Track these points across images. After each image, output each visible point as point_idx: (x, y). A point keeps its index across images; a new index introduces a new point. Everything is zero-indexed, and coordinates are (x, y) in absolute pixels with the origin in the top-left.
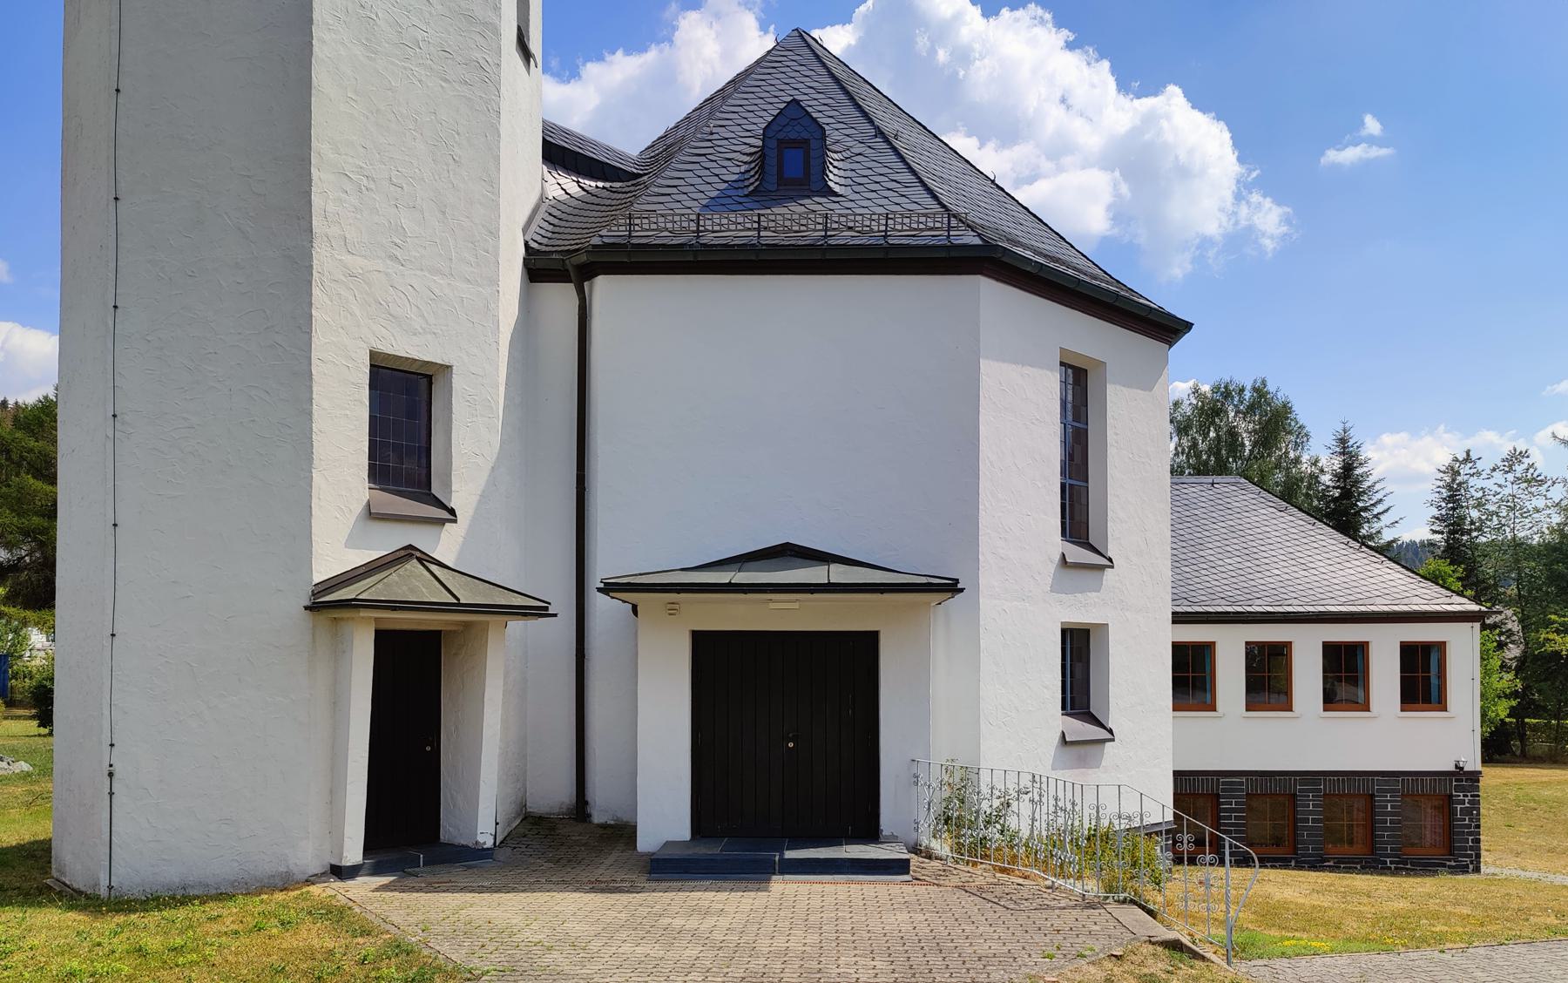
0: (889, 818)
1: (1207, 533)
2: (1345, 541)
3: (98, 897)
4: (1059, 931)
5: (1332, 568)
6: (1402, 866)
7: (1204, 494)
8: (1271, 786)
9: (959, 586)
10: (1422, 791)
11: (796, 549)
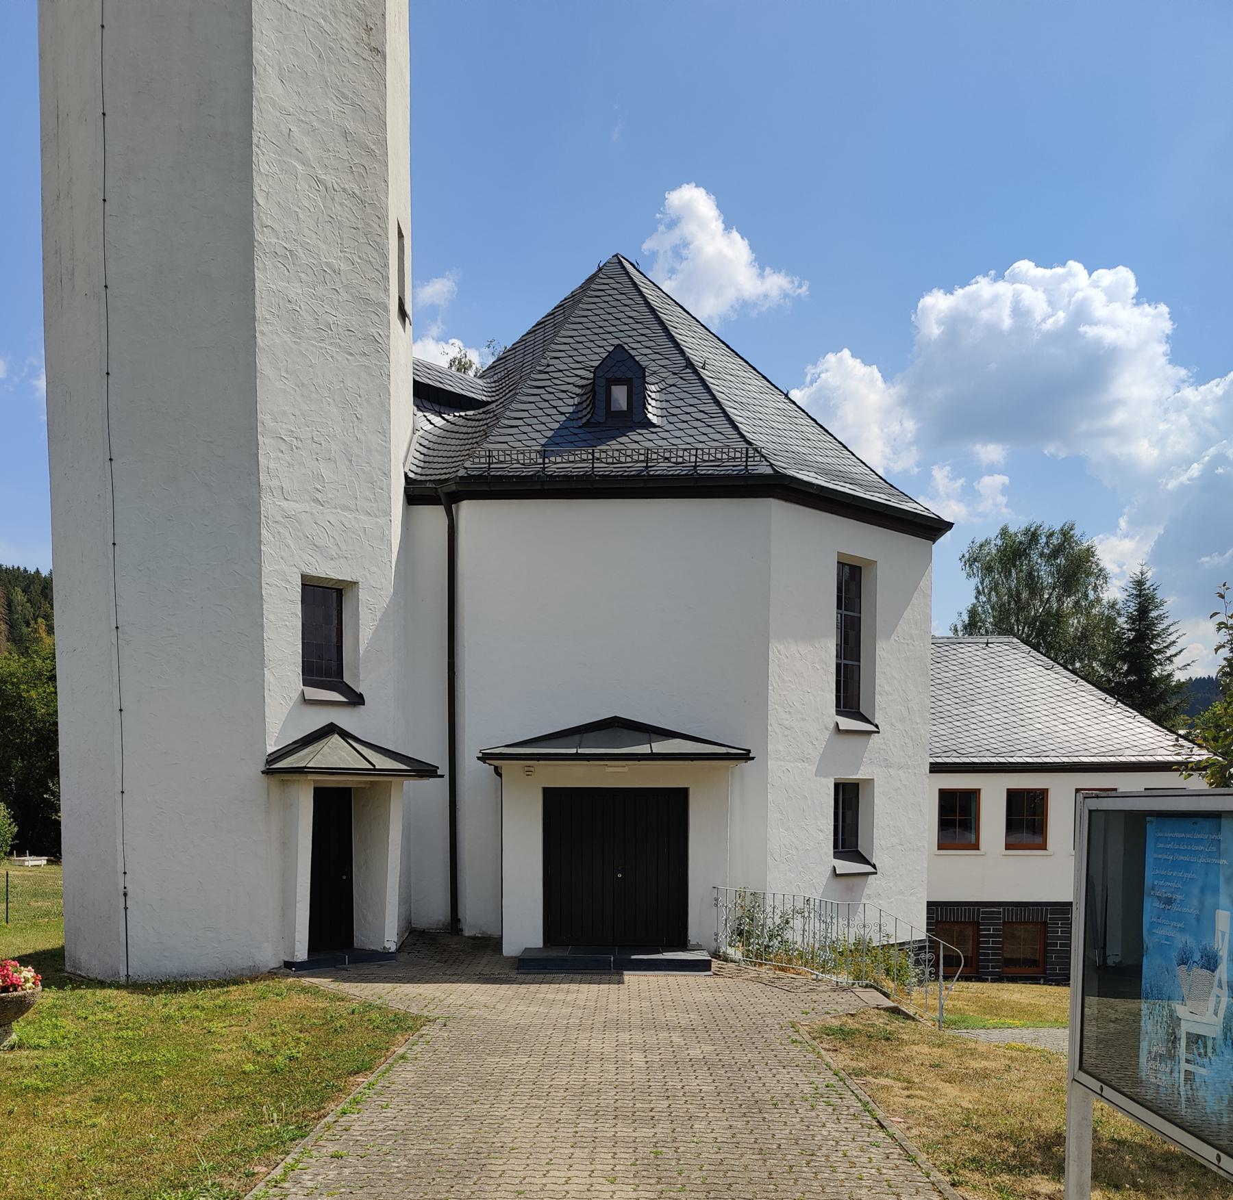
1: (979, 690)
2: (1103, 697)
5: (1088, 722)
7: (978, 653)
9: (751, 755)
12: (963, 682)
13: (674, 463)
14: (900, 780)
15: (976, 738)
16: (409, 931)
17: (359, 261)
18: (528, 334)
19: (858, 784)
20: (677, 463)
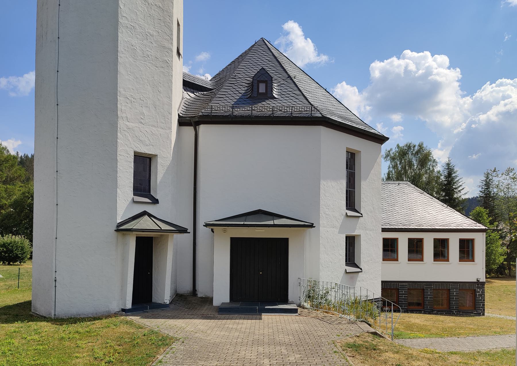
0: (291, 296)
1: (396, 201)
3: (51, 318)
4: (342, 329)
6: (458, 313)
7: (396, 187)
8: (416, 286)
9: (314, 226)
10: (466, 288)
11: (263, 211)
12: (390, 198)
13: (283, 112)
15: (396, 219)
16: (176, 295)
17: (161, 32)
18: (228, 65)
19: (354, 237)
20: (284, 112)
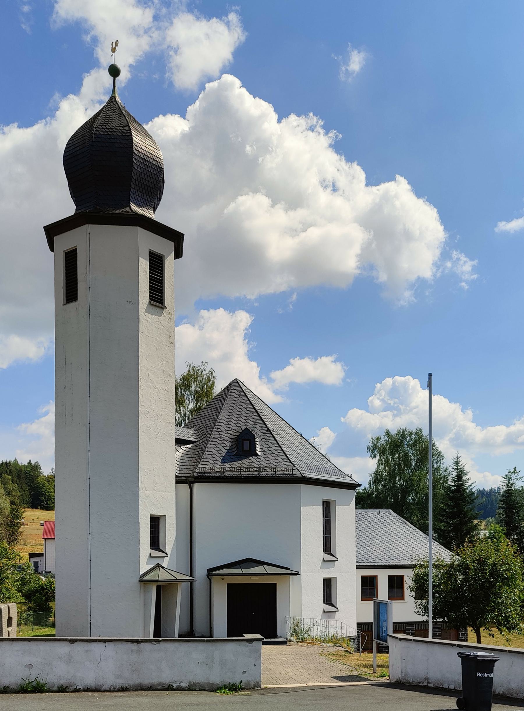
0: (279, 632)
1: (376, 533)
2: (425, 537)
14: (346, 577)
